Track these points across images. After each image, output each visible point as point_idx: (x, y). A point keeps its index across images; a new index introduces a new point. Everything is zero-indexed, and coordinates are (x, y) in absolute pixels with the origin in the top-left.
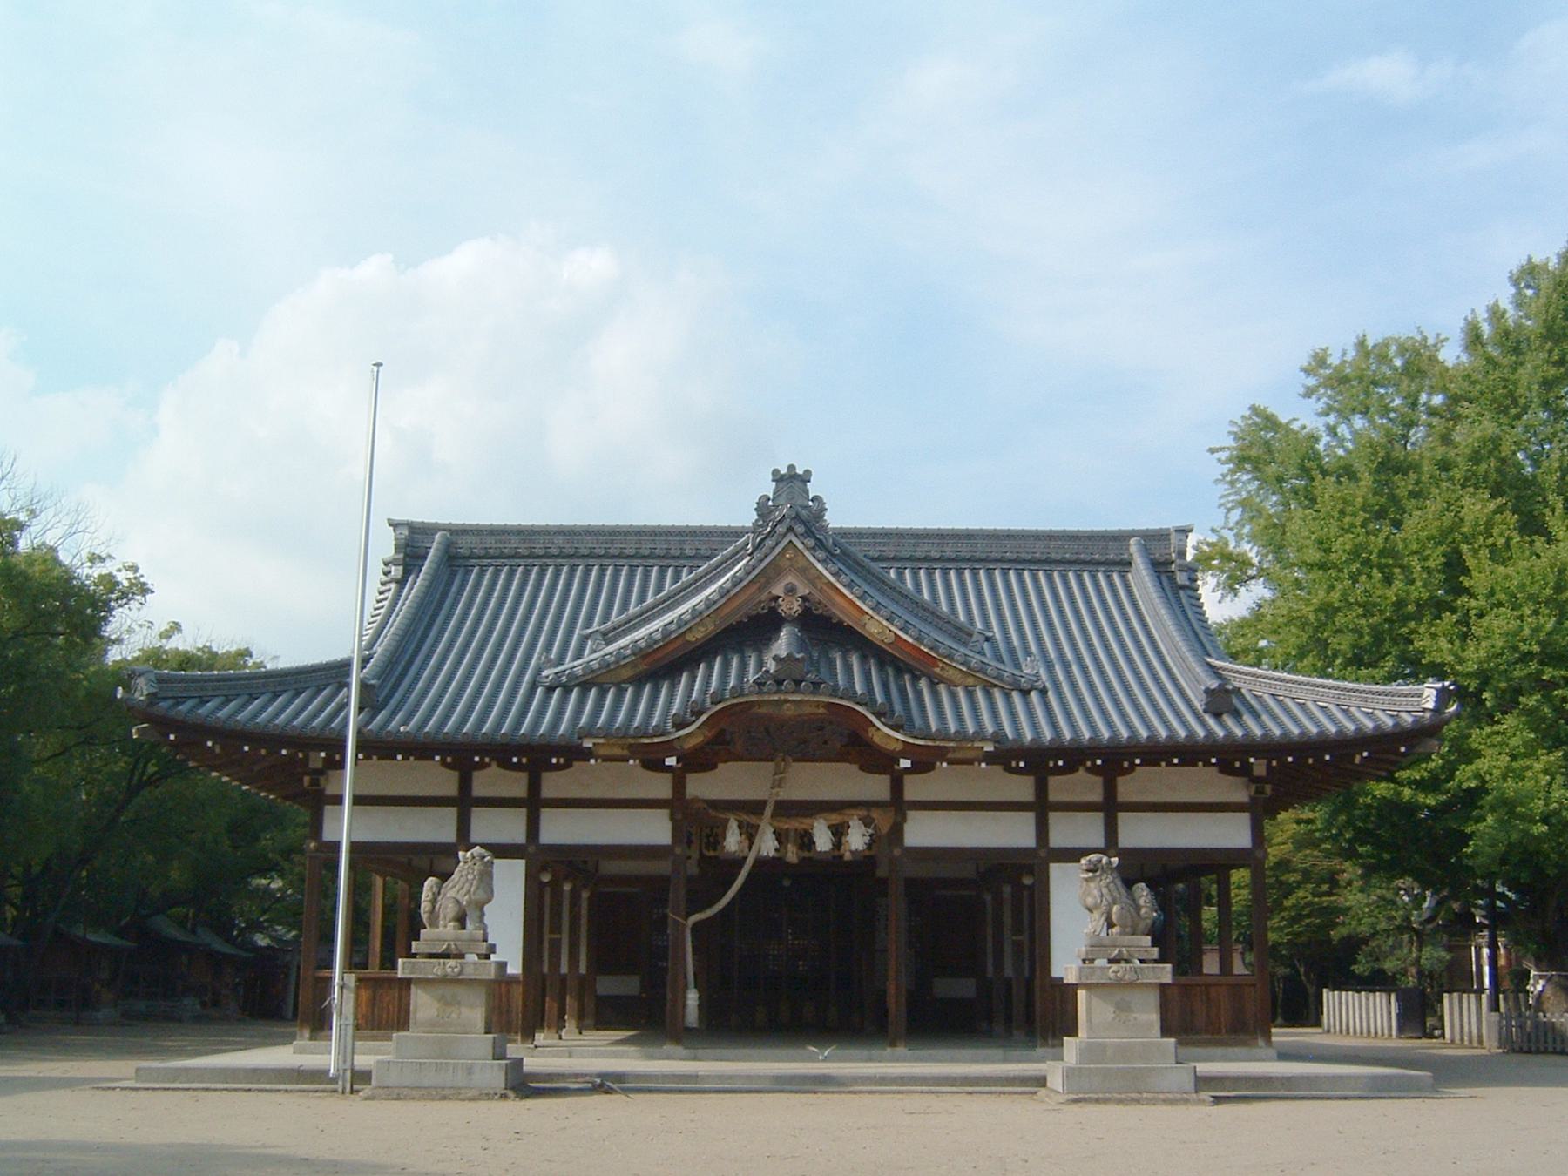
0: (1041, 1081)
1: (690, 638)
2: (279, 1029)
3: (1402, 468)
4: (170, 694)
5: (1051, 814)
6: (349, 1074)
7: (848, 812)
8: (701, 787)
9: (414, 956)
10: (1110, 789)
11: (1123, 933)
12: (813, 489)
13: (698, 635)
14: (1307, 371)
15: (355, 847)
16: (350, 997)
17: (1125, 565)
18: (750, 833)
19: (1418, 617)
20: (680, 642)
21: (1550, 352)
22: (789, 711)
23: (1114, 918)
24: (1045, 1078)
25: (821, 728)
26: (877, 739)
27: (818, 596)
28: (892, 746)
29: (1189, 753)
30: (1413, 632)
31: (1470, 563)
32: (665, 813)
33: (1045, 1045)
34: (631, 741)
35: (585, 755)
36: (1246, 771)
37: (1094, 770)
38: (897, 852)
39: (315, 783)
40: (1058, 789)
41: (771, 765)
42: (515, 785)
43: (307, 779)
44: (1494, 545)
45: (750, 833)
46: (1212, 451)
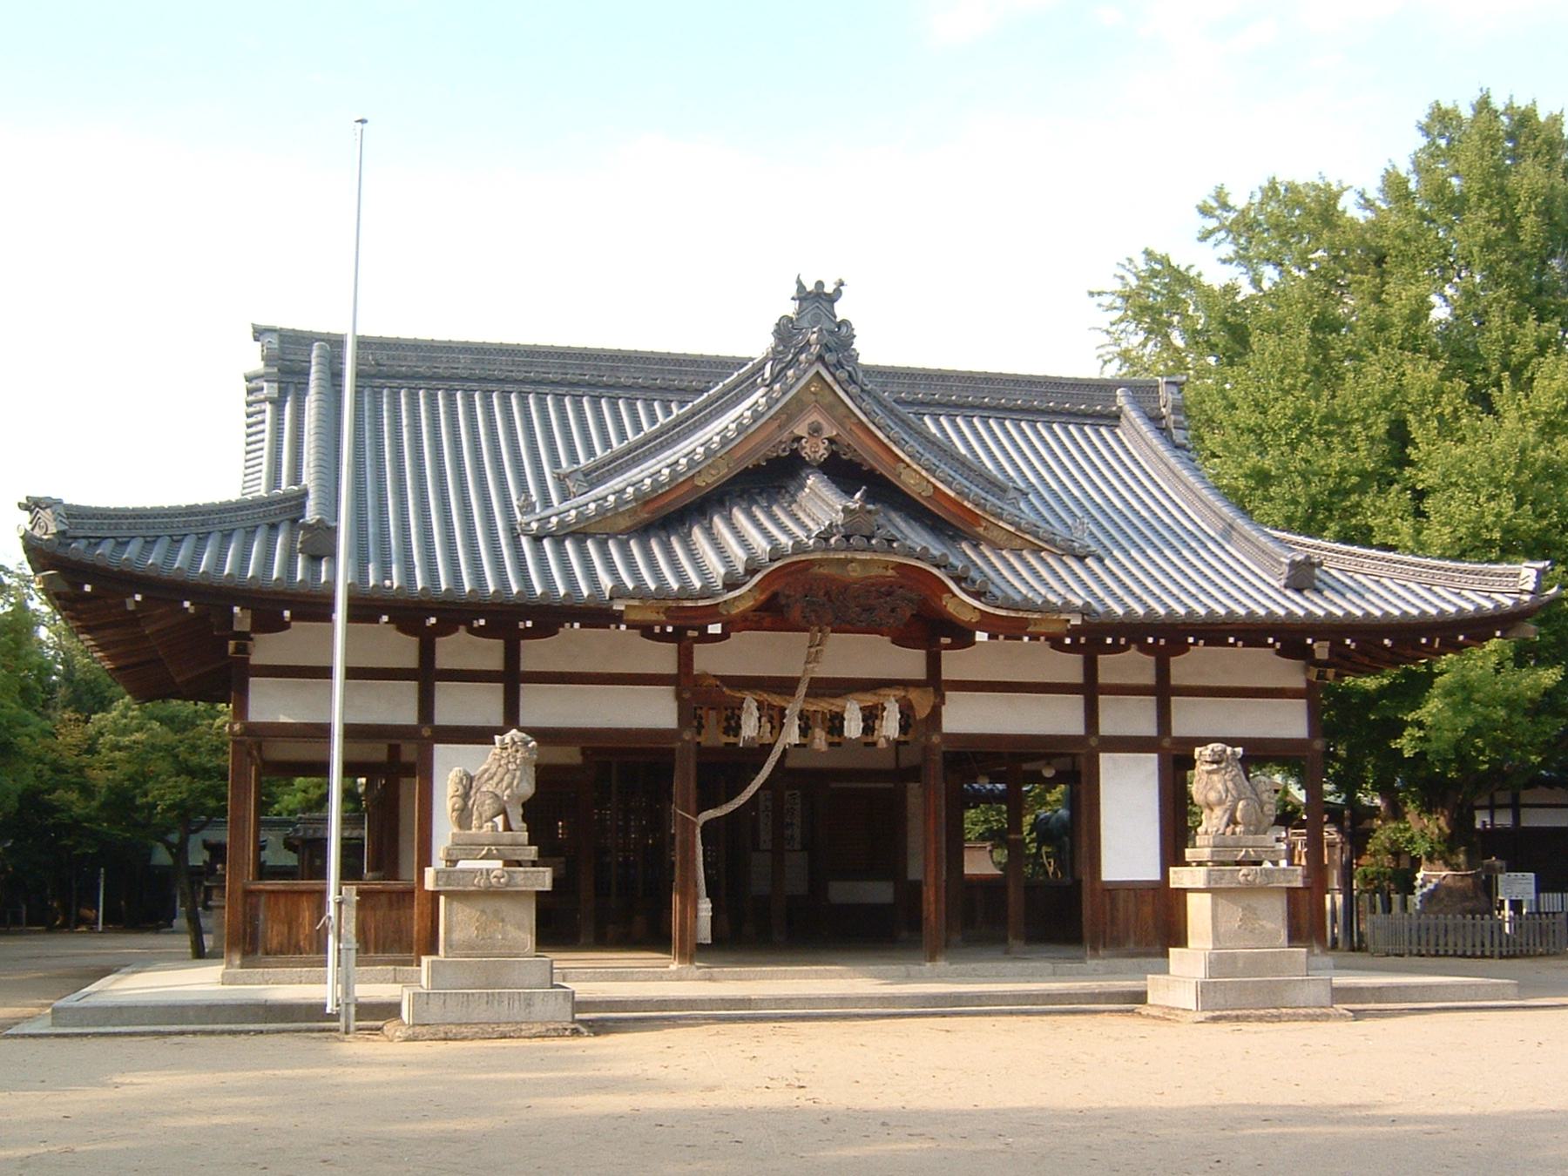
0: (1140, 997)
1: (700, 482)
2: (1072, 951)
4: (80, 533)
5: (440, 686)
6: (353, 1009)
7: (911, 689)
9: (1188, 864)
10: (1163, 671)
11: (1246, 832)
13: (706, 481)
14: (1205, 211)
15: (353, 733)
16: (350, 914)
19: (1361, 489)
20: (686, 488)
21: (1489, 209)
22: (855, 572)
23: (1238, 814)
24: (1145, 993)
27: (847, 439)
28: (967, 617)
29: (1252, 632)
30: (1358, 505)
32: (668, 691)
33: (1095, 956)
34: (670, 603)
35: (617, 618)
36: (1305, 654)
37: (1145, 649)
38: (936, 739)
39: (243, 649)
40: (1111, 668)
41: (902, 765)
42: (490, 654)
43: (232, 644)
44: (1442, 414)
45: (776, 719)
46: (1091, 294)
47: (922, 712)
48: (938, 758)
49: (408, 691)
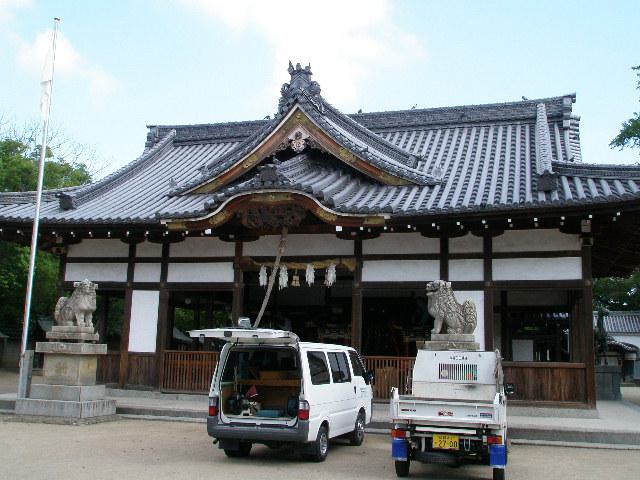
5: (494, 261)
7: (328, 261)
12: (313, 78)
17: (532, 120)
25: (290, 209)
26: (322, 215)
28: (329, 219)
32: (231, 264)
37: (124, 239)
40: (455, 245)
42: (156, 250)
49: (479, 264)
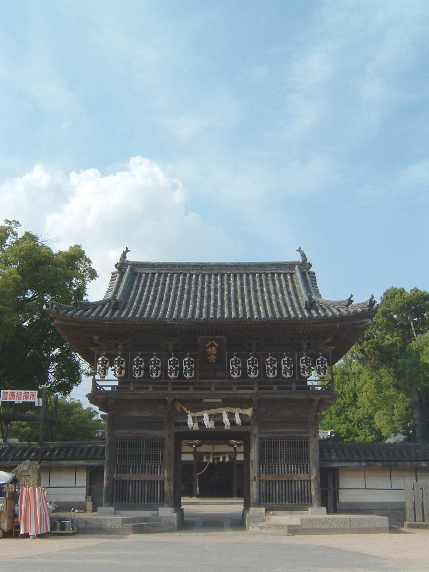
3: (347, 374)
8: (199, 449)
18: (208, 458)
19: (348, 407)
31: (358, 396)
41: (212, 446)
45: (208, 458)
47: (233, 457)
48: (314, 499)
